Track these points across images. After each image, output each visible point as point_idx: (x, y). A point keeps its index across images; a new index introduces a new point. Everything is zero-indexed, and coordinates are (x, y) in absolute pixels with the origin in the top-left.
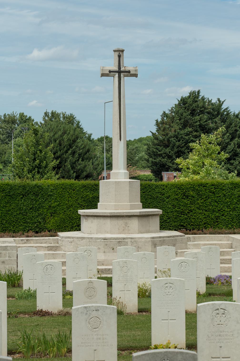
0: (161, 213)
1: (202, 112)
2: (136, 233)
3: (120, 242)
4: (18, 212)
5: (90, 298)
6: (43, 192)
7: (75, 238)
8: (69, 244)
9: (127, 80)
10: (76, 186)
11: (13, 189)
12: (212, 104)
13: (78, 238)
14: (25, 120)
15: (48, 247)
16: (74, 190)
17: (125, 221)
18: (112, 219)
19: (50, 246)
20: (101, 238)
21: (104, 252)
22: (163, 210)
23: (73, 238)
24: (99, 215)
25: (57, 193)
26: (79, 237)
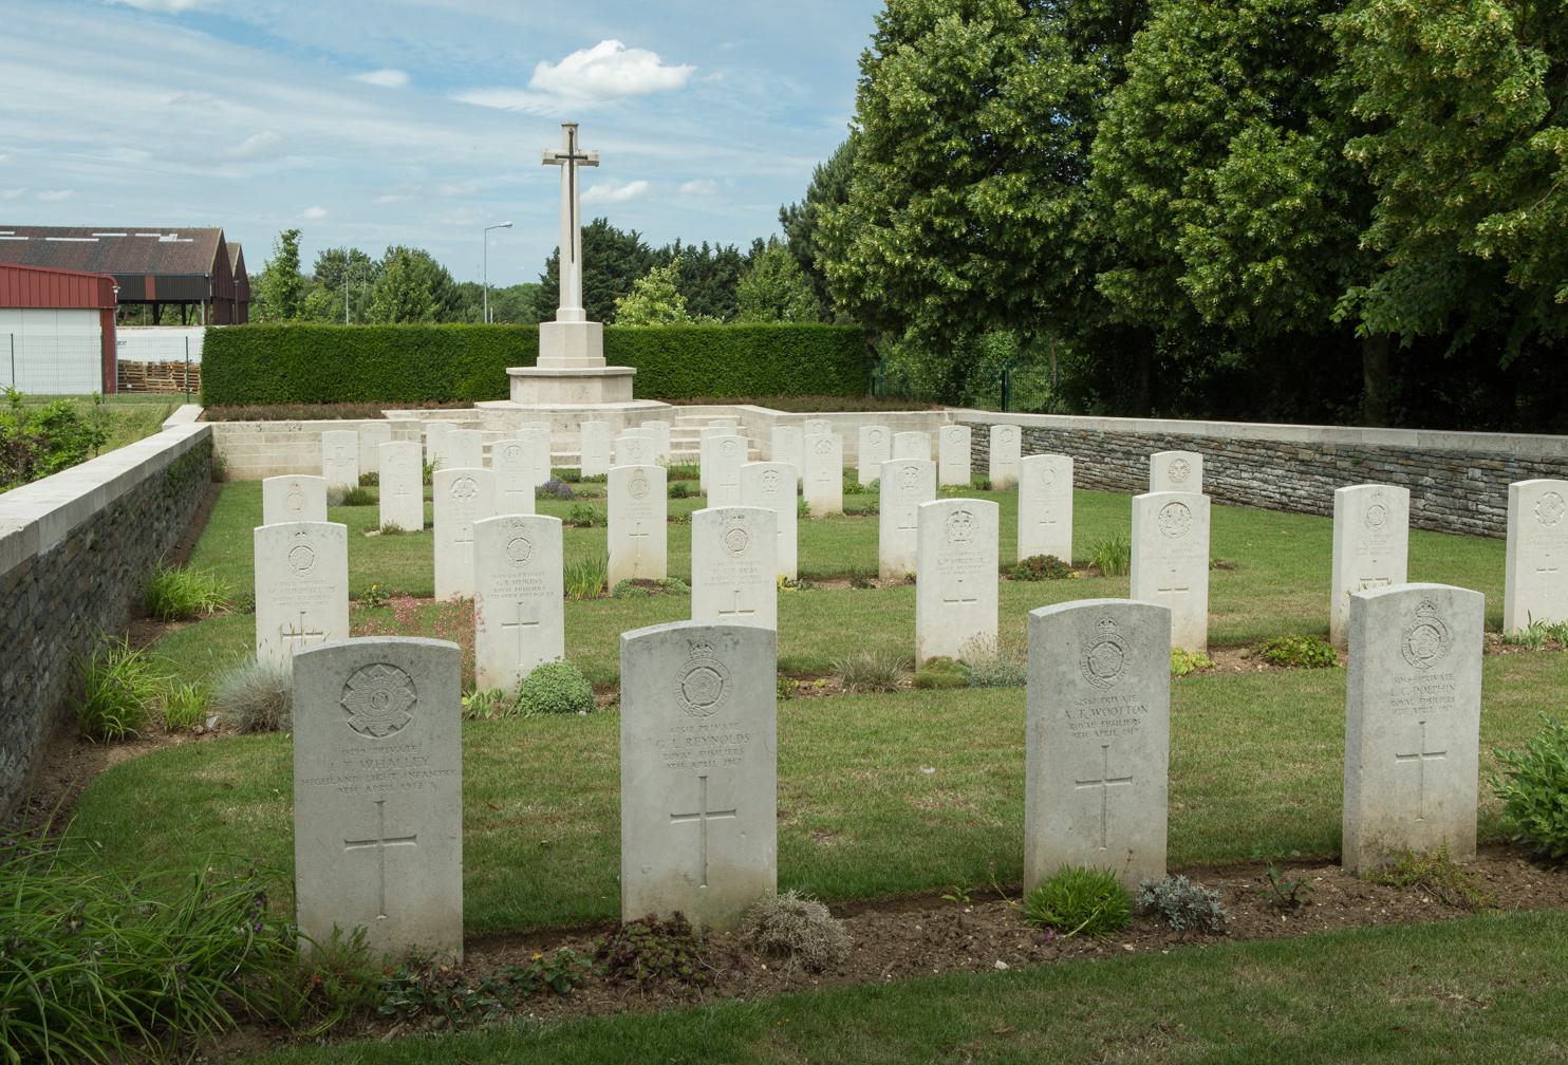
13: (510, 410)
14: (358, 258)
22: (639, 366)
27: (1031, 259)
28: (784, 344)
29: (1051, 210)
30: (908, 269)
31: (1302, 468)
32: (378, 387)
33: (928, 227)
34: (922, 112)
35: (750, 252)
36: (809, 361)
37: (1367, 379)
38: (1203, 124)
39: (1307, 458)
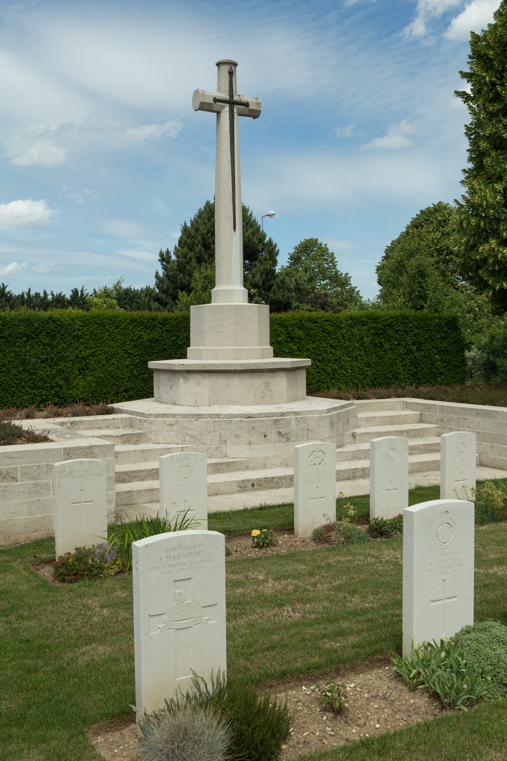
2: (283, 403)
3: (278, 422)
4: (21, 369)
6: (64, 330)
7: (178, 417)
8: (168, 428)
10: (121, 321)
11: (8, 325)
13: (185, 416)
15: (122, 436)
16: (117, 328)
17: (265, 380)
18: (243, 375)
19: (125, 435)
20: (241, 416)
21: (250, 443)
23: (174, 416)
24: (217, 369)
25: (88, 333)
26: (190, 415)
35: (71, 296)
36: (418, 350)
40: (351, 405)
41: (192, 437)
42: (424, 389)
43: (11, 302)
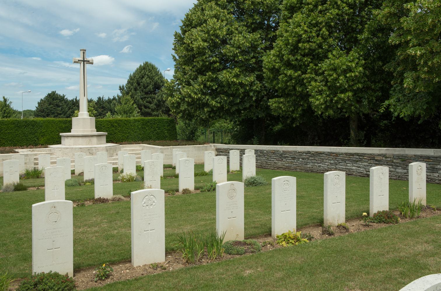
0: (107, 134)
1: (57, 99)
4: (23, 135)
5: (231, 198)
8: (59, 151)
9: (87, 66)
12: (61, 96)
13: (64, 148)
17: (90, 139)
18: (83, 137)
23: (61, 148)
27: (240, 96)
28: (151, 124)
29: (247, 80)
30: (199, 99)
31: (377, 162)
32: (10, 141)
33: (205, 86)
34: (204, 48)
35: (97, 101)
37: (352, 132)
38: (314, 50)
39: (380, 159)
40: (118, 146)
41: (65, 154)
42: (157, 142)
43: (67, 103)
